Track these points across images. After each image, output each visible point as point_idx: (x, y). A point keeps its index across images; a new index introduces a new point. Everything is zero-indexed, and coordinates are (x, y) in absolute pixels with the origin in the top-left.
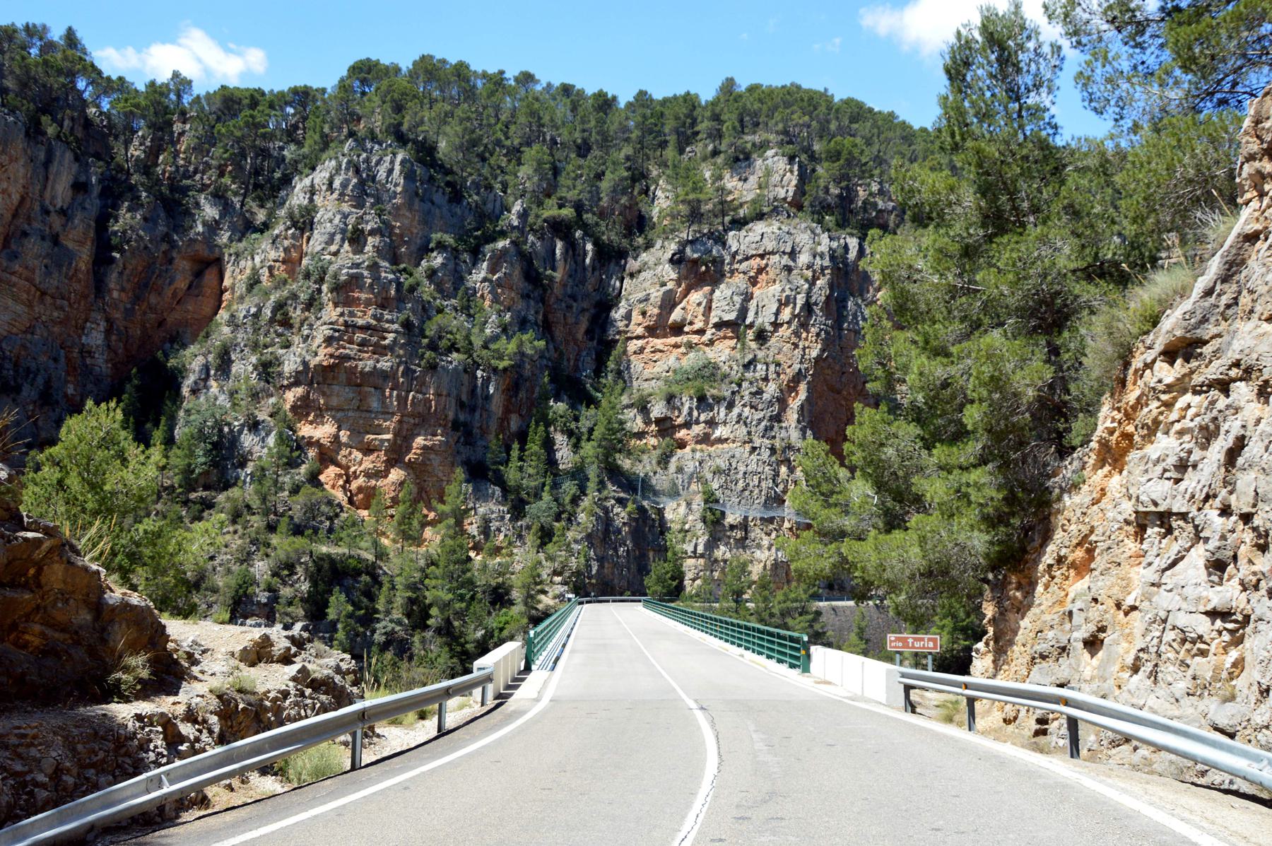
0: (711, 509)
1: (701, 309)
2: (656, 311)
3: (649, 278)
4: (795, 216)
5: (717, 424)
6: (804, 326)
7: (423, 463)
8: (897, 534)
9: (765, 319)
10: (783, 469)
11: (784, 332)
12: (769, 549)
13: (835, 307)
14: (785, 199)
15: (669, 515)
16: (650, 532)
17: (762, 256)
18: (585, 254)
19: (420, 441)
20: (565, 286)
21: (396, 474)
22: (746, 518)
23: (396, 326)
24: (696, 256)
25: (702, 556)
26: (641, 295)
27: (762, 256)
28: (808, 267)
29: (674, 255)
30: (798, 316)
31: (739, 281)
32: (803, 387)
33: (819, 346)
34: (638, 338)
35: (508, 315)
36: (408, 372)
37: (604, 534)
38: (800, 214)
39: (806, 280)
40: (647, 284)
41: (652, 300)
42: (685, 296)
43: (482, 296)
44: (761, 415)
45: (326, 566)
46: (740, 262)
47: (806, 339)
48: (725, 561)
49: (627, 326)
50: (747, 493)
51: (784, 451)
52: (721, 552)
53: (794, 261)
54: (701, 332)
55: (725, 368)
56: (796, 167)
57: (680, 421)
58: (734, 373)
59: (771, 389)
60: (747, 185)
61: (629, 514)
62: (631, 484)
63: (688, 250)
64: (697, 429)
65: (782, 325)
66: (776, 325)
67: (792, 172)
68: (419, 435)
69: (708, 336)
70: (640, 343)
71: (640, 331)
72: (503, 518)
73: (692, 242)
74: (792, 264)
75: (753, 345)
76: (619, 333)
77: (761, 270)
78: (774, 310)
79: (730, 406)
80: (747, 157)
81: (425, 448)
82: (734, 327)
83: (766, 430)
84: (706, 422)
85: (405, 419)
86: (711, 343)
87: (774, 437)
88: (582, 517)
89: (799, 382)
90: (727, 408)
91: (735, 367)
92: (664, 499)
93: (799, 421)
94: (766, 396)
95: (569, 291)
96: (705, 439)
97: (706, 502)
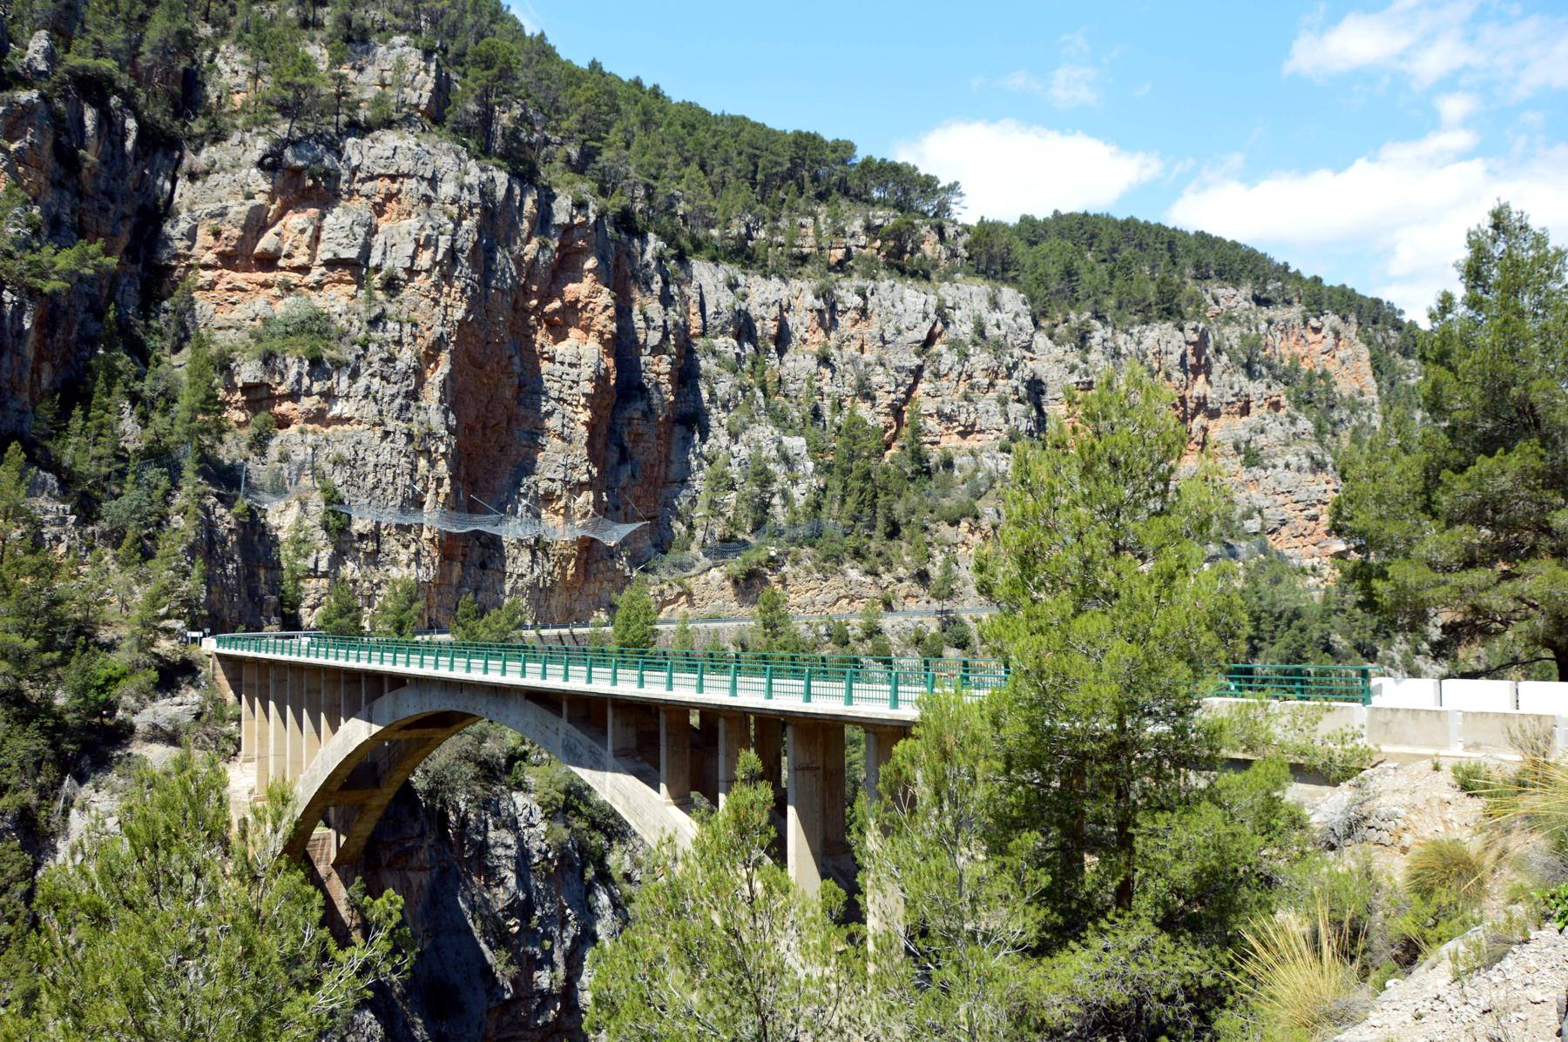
0: (334, 512)
1: (306, 238)
2: (237, 232)
3: (217, 190)
4: (431, 131)
5: (336, 398)
6: (447, 277)
8: (896, 542)
9: (397, 262)
10: (422, 463)
11: (422, 282)
12: (408, 566)
13: (483, 258)
14: (417, 106)
15: (272, 520)
16: (256, 538)
17: (393, 178)
18: (124, 134)
20: (96, 176)
22: (378, 524)
24: (300, 163)
25: (325, 575)
26: (214, 207)
27: (393, 178)
29: (265, 157)
30: (440, 263)
31: (360, 207)
32: (444, 357)
33: (464, 306)
34: (206, 267)
35: (36, 211)
37: (207, 546)
38: (435, 129)
39: (451, 218)
40: (223, 193)
42: (280, 217)
44: (394, 389)
46: (362, 181)
47: (448, 295)
48: (354, 582)
49: (189, 248)
50: (378, 492)
51: (423, 440)
52: (349, 569)
53: (434, 190)
54: (304, 270)
55: (342, 322)
56: (433, 66)
57: (281, 389)
58: (354, 330)
59: (406, 357)
60: (362, 79)
61: (237, 516)
62: (227, 479)
63: (288, 153)
64: (308, 403)
65: (418, 273)
66: (412, 272)
67: (427, 71)
69: (315, 274)
70: (209, 275)
72: (63, 521)
73: (295, 143)
74: (431, 194)
75: (380, 295)
76: (177, 256)
77: (390, 197)
79: (354, 375)
80: (364, 40)
82: (355, 268)
83: (401, 410)
84: (321, 394)
86: (319, 286)
87: (410, 420)
88: (178, 521)
89: (439, 350)
90: (350, 377)
91: (357, 323)
92: (265, 497)
93: (441, 401)
94: (400, 365)
95: (102, 184)
96: (319, 417)
97: (328, 502)
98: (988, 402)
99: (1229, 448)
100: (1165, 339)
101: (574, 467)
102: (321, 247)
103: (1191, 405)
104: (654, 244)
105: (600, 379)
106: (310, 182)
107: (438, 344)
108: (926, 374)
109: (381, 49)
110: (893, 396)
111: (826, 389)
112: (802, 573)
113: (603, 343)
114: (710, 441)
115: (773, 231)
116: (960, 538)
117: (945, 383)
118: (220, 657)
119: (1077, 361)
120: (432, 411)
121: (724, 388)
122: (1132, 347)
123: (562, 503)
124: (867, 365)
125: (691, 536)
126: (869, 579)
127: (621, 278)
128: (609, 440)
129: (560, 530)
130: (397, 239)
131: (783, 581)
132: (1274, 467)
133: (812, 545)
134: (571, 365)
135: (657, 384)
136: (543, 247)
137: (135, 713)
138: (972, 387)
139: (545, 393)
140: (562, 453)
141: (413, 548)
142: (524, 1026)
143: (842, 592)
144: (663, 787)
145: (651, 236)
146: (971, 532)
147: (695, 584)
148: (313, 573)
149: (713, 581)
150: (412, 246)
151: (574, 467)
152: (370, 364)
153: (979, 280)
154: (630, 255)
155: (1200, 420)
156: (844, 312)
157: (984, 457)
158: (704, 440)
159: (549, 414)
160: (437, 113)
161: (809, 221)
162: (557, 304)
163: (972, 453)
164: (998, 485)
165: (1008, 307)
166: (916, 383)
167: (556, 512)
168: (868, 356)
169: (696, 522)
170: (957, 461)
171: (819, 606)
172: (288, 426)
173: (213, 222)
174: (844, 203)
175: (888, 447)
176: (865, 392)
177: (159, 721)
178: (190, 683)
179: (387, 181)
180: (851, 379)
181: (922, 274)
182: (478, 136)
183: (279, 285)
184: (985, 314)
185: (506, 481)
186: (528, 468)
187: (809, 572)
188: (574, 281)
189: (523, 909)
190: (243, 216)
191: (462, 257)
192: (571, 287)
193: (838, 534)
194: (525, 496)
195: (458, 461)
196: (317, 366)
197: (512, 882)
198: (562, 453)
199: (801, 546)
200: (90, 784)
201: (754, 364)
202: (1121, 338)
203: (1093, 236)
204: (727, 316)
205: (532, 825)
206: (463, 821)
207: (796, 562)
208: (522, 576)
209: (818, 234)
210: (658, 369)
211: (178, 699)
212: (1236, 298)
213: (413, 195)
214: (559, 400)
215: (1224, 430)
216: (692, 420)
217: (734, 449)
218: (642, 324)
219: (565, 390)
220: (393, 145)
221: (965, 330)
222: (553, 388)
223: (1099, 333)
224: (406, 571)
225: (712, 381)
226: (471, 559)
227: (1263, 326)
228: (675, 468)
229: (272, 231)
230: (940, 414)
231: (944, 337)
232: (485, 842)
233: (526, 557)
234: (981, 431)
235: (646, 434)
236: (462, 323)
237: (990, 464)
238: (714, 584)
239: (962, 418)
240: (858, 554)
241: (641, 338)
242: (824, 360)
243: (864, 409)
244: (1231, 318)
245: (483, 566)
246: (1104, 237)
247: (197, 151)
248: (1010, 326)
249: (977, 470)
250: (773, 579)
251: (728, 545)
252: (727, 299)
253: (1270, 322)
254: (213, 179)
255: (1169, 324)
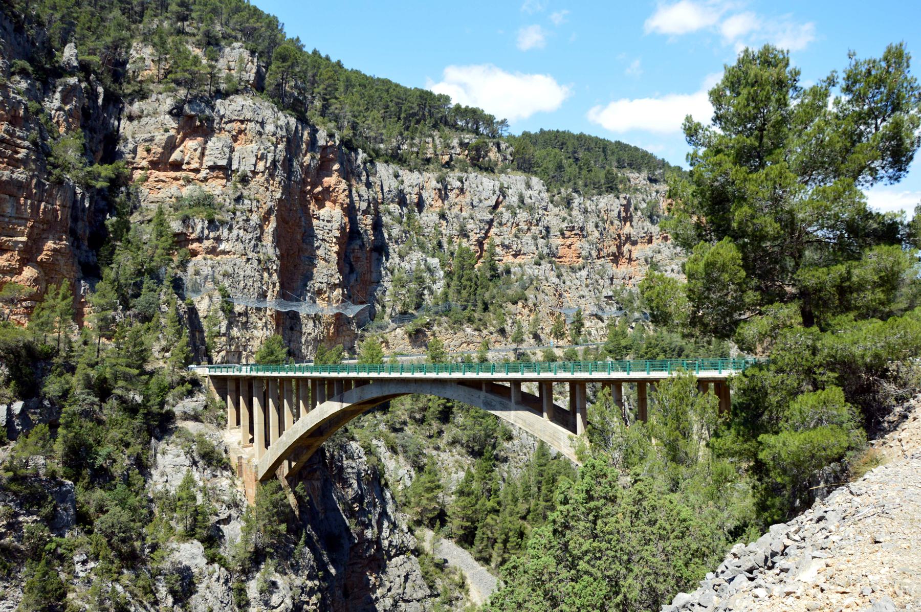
0: (227, 302)
2: (160, 150)
3: (146, 126)
6: (272, 175)
7: (53, 263)
8: (487, 313)
9: (246, 167)
10: (266, 275)
11: (260, 178)
13: (288, 164)
14: (248, 81)
17: (242, 122)
18: (97, 96)
19: (50, 244)
21: (29, 272)
23: (26, 143)
24: (193, 113)
25: (224, 335)
27: (242, 122)
28: (274, 135)
31: (225, 137)
32: (273, 218)
34: (142, 168)
36: (39, 185)
39: (273, 144)
41: (156, 141)
43: (58, 122)
45: (23, 352)
46: (226, 123)
48: (238, 338)
49: (134, 158)
50: (246, 290)
52: (235, 332)
54: (197, 171)
55: (220, 199)
56: (255, 60)
57: (193, 236)
58: (227, 204)
59: (255, 218)
63: (186, 107)
64: (207, 244)
65: (258, 173)
66: (255, 173)
67: (253, 62)
68: (47, 239)
69: (203, 173)
71: (144, 163)
75: (239, 186)
76: (128, 163)
77: (240, 132)
78: (254, 162)
79: (230, 229)
81: (54, 250)
82: (225, 171)
84: (214, 239)
85: (36, 224)
86: (205, 180)
91: (228, 200)
94: (252, 223)
96: (213, 251)
97: (224, 296)
98: (527, 238)
99: (642, 261)
100: (609, 203)
101: (332, 276)
102: (205, 158)
103: (623, 238)
104: (362, 156)
105: (342, 229)
106: (198, 123)
107: (269, 212)
108: (495, 223)
109: (227, 50)
110: (478, 235)
111: (444, 232)
112: (443, 330)
113: (343, 209)
114: (390, 260)
115: (412, 145)
116: (518, 311)
117: (505, 228)
118: (211, 376)
119: (566, 215)
120: (269, 248)
121: (396, 231)
122: (594, 208)
123: (326, 295)
124: (464, 219)
125: (384, 312)
126: (477, 333)
127: (349, 173)
128: (346, 262)
129: (327, 309)
130: (245, 155)
131: (434, 335)
132: (666, 271)
133: (446, 316)
134: (328, 221)
135: (366, 230)
136: (313, 158)
137: (173, 406)
138: (519, 230)
139: (316, 237)
140: (326, 270)
141: (264, 320)
142: (360, 557)
143: (464, 340)
144: (545, 414)
145: (360, 151)
146: (524, 307)
147: (390, 337)
148: (219, 334)
149: (398, 335)
150: (255, 159)
151: (332, 276)
152: (238, 222)
153: (520, 173)
154: (349, 160)
155: (627, 247)
156: (451, 190)
157: (526, 267)
158: (387, 260)
159: (318, 248)
160: (259, 86)
161: (430, 140)
162: (320, 189)
163: (520, 265)
164: (535, 282)
165: (535, 188)
166: (490, 228)
167: (323, 300)
168: (464, 214)
169: (387, 304)
170: (513, 270)
171: (452, 347)
172: (196, 256)
173: (147, 144)
174: (447, 130)
175: (476, 263)
176: (464, 234)
177: (186, 410)
178: (199, 391)
179: (239, 123)
180: (457, 226)
181: (489, 169)
182: (281, 100)
183: (183, 179)
184: (524, 191)
185: (299, 283)
186: (310, 277)
187: (447, 330)
188: (327, 176)
189: (359, 498)
190: (164, 141)
191: (279, 165)
192: (326, 179)
193: (459, 308)
194: (309, 291)
195: (282, 273)
196: (213, 224)
197: (355, 486)
198: (326, 270)
199: (441, 316)
200: (164, 442)
201: (409, 218)
202: (588, 203)
203: (563, 144)
204: (395, 192)
205: (360, 458)
206: (332, 456)
207: (440, 325)
208: (310, 334)
209: (435, 147)
210: (365, 222)
211: (195, 399)
212: (638, 178)
213: (251, 132)
214: (322, 240)
215: (640, 251)
216: (381, 249)
217: (403, 264)
218: (357, 198)
219: (326, 235)
220: (241, 104)
221: (513, 200)
222: (319, 233)
223: (577, 200)
224: (261, 332)
225: (389, 228)
226: (288, 324)
227: (654, 194)
228: (374, 275)
229: (178, 150)
230: (503, 245)
231: (504, 204)
232: (342, 466)
233: (311, 324)
234: (524, 254)
235: (362, 255)
236: (280, 200)
237: (530, 271)
238: (399, 336)
239: (514, 247)
240: (470, 320)
241: (357, 205)
242: (443, 216)
243: (465, 244)
244: (637, 190)
245: (292, 329)
246: (569, 144)
247: (131, 103)
248: (536, 198)
249: (523, 275)
250: (429, 333)
251: (403, 317)
252: (394, 184)
253: (657, 192)
254: (144, 120)
255: (612, 195)
